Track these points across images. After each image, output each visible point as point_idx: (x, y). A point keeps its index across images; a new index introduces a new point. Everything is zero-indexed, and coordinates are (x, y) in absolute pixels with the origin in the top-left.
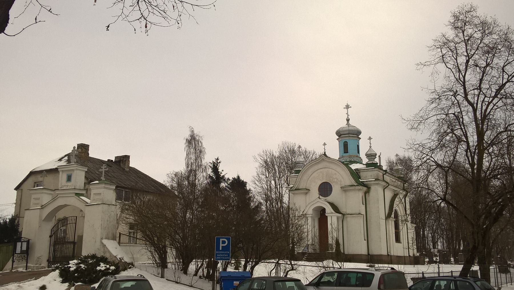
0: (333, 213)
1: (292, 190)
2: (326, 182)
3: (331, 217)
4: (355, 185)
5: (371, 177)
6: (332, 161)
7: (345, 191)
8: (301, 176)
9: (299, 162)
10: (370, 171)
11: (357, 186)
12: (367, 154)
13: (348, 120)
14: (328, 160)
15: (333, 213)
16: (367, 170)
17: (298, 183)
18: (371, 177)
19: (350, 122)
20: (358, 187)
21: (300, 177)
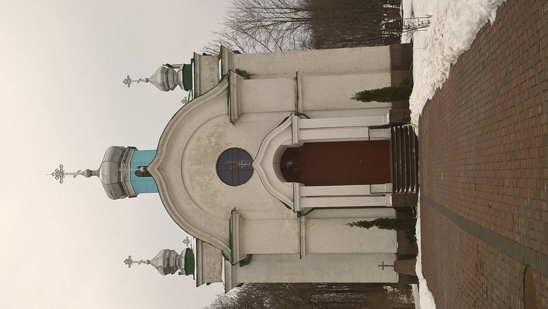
0: (291, 125)
1: (232, 255)
2: (217, 166)
3: (302, 131)
4: (227, 85)
5: (213, 69)
6: (165, 145)
7: (241, 115)
8: (195, 230)
9: (166, 259)
10: (200, 82)
11: (229, 81)
12: (163, 84)
13: (90, 173)
14: (162, 157)
15: (291, 125)
16: (198, 79)
17: (214, 239)
18: (213, 69)
19: (94, 168)
20: (233, 79)
21: (200, 232)
